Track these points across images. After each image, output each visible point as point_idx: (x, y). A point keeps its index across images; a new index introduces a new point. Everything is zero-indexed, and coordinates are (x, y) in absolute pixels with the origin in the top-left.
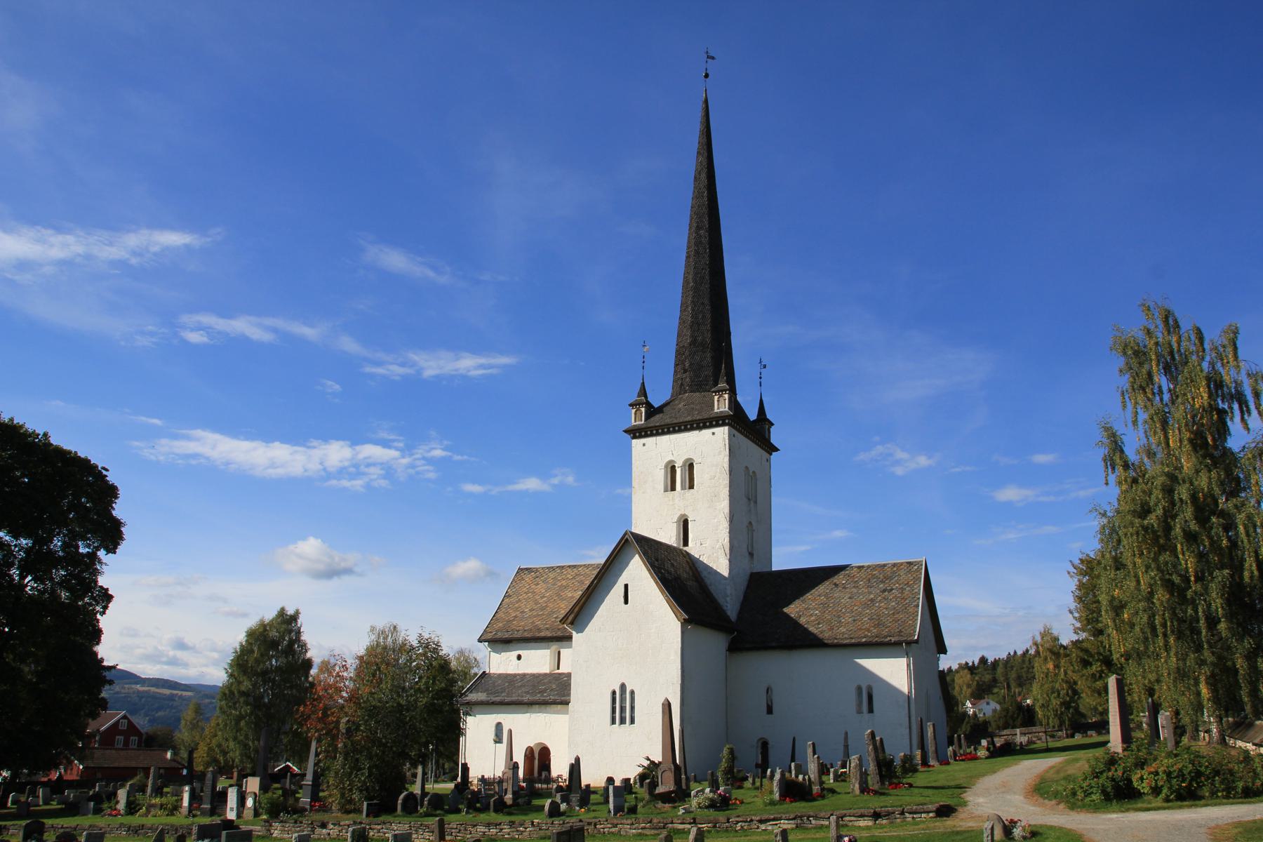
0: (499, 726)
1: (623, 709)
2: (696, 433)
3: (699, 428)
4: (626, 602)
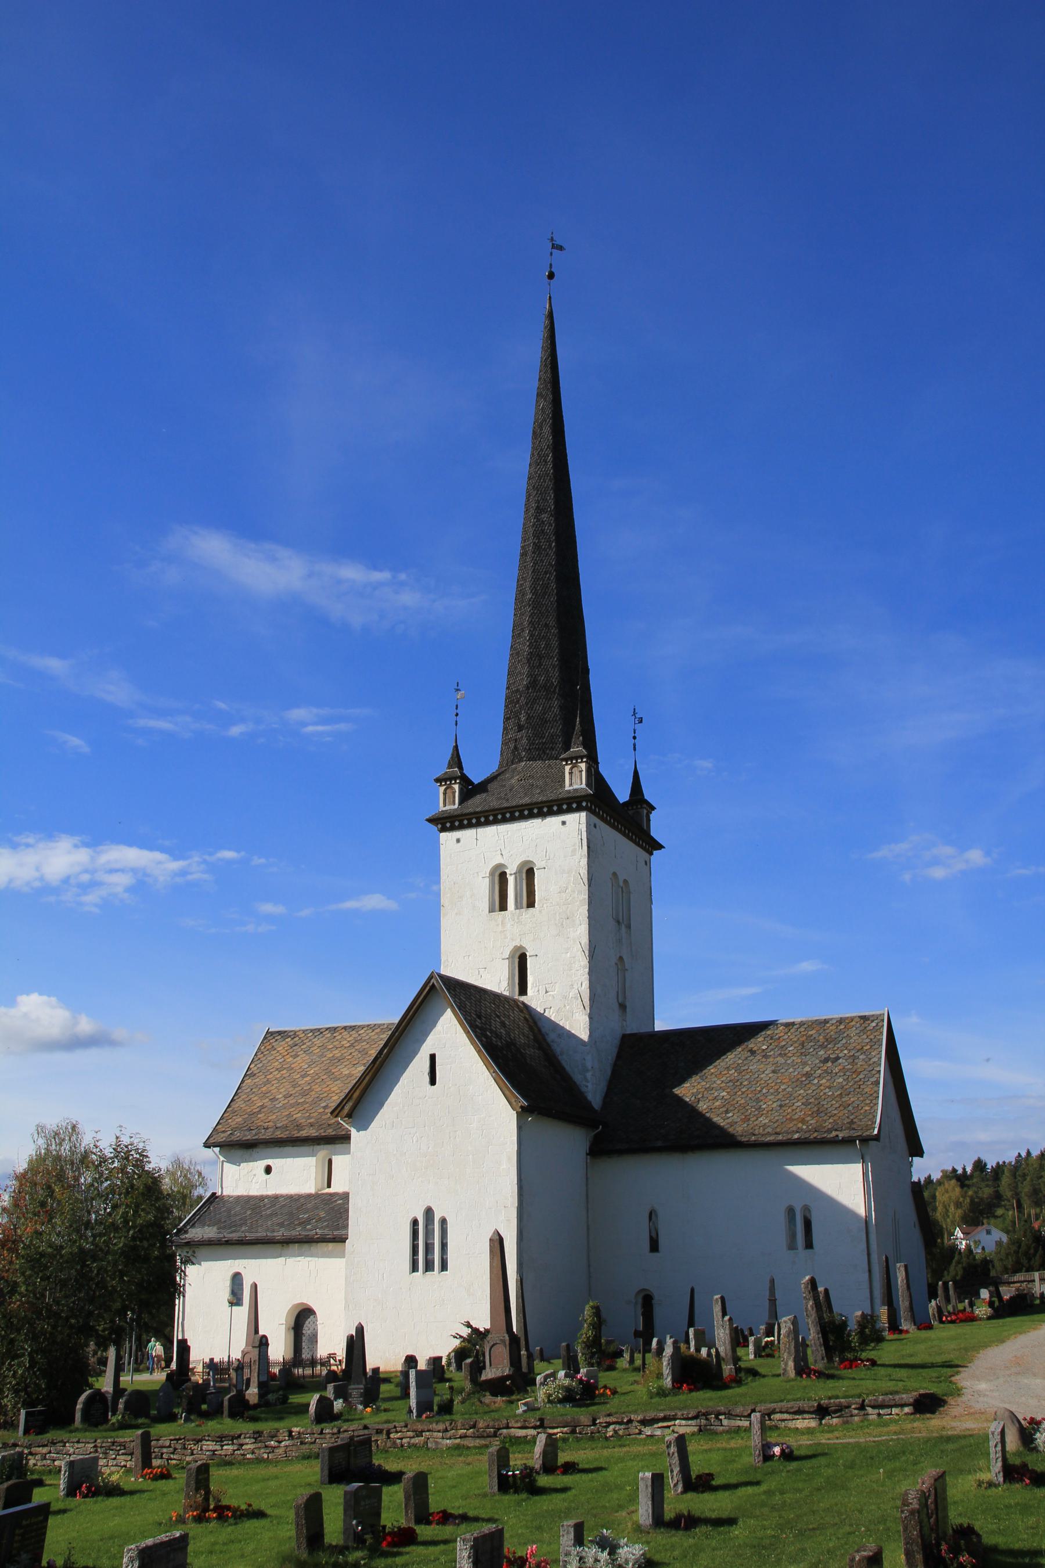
0: (237, 1279)
2: (537, 822)
4: (433, 1081)
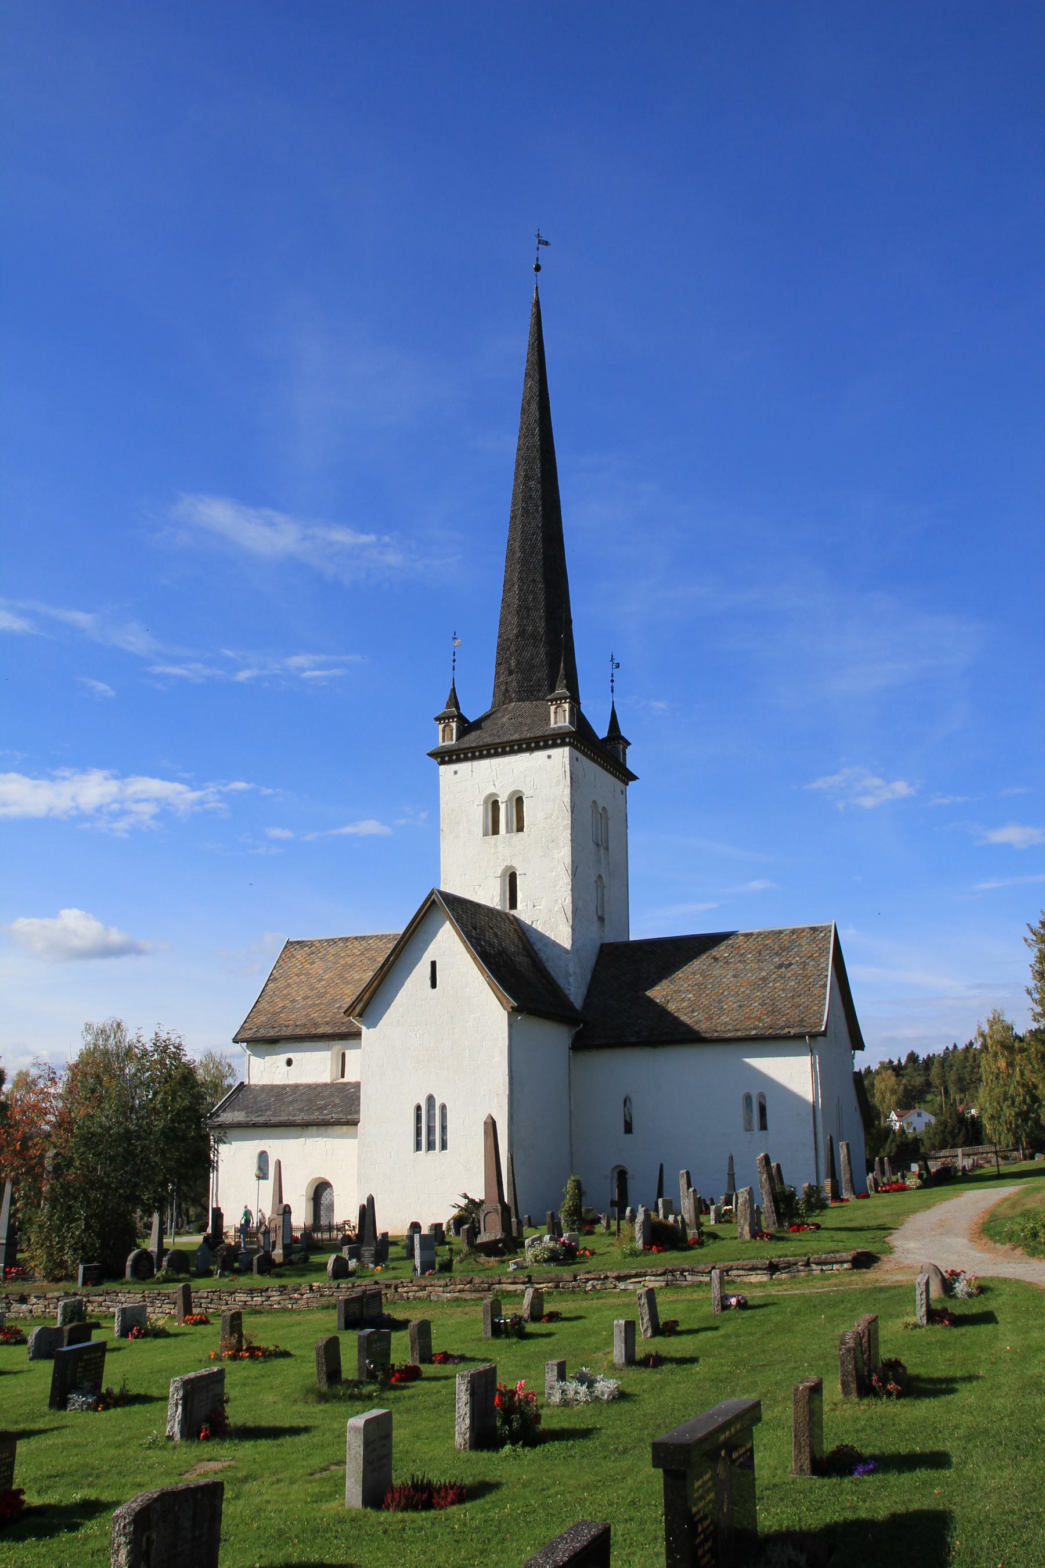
0: (263, 1156)
1: (430, 1130)
3: (530, 749)
4: (434, 985)
